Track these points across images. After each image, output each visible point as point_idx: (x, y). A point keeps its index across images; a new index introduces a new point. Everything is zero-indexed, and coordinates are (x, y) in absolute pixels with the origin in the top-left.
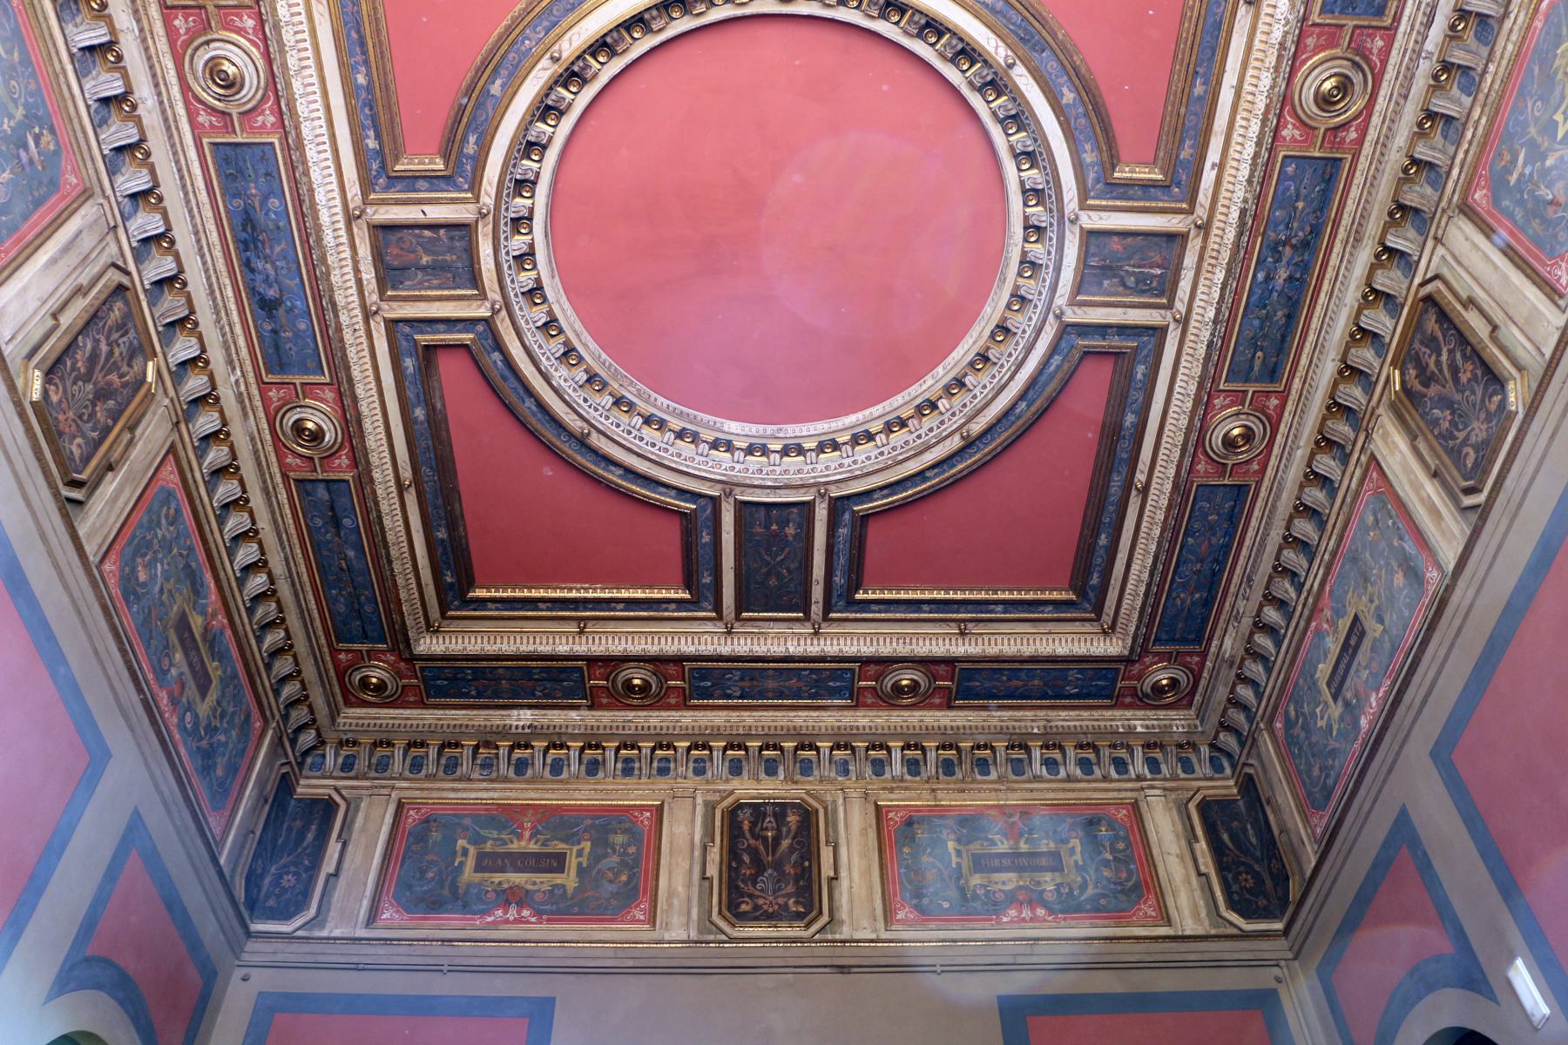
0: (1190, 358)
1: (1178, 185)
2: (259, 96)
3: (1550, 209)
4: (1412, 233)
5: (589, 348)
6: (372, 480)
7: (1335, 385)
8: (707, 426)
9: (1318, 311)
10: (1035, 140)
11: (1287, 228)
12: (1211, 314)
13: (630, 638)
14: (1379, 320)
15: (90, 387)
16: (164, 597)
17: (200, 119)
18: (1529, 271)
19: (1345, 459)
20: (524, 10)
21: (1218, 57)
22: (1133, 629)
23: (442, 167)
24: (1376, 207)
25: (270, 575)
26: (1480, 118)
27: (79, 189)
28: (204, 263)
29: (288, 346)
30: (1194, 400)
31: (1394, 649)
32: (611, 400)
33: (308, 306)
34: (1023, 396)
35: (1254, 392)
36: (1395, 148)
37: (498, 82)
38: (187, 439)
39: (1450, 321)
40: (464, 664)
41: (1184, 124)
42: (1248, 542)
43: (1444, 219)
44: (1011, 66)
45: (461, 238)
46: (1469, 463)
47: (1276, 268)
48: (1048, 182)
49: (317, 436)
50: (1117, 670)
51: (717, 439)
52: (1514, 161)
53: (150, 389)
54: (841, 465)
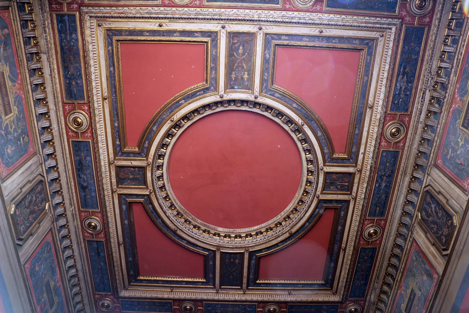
0: (357, 210)
1: (352, 159)
2: (87, 128)
3: (460, 166)
4: (421, 172)
5: (178, 204)
6: (110, 242)
7: (401, 217)
8: (212, 229)
9: (395, 195)
10: (310, 146)
11: (384, 171)
12: (363, 196)
13: (187, 294)
14: (413, 198)
15: (29, 210)
16: (43, 276)
17: (70, 134)
18: (456, 184)
19: (405, 240)
20: (164, 107)
21: (362, 123)
22: (342, 293)
23: (138, 150)
24: (410, 165)
25: (77, 269)
26: (437, 140)
27: (33, 152)
28: (66, 175)
29: (89, 200)
30: (359, 222)
31: (425, 300)
32: (184, 220)
33: (95, 189)
34: (307, 221)
35: (377, 219)
36: (414, 148)
37: (155, 127)
38: (56, 227)
39: (434, 198)
40: (135, 300)
41: (353, 141)
42: (377, 265)
43: (430, 169)
44: (303, 125)
45: (142, 171)
46: (444, 241)
47: (381, 183)
48: (314, 158)
49: (95, 227)
50: (338, 306)
51: (215, 233)
52: (448, 152)
53: (46, 211)
54: (253, 242)
